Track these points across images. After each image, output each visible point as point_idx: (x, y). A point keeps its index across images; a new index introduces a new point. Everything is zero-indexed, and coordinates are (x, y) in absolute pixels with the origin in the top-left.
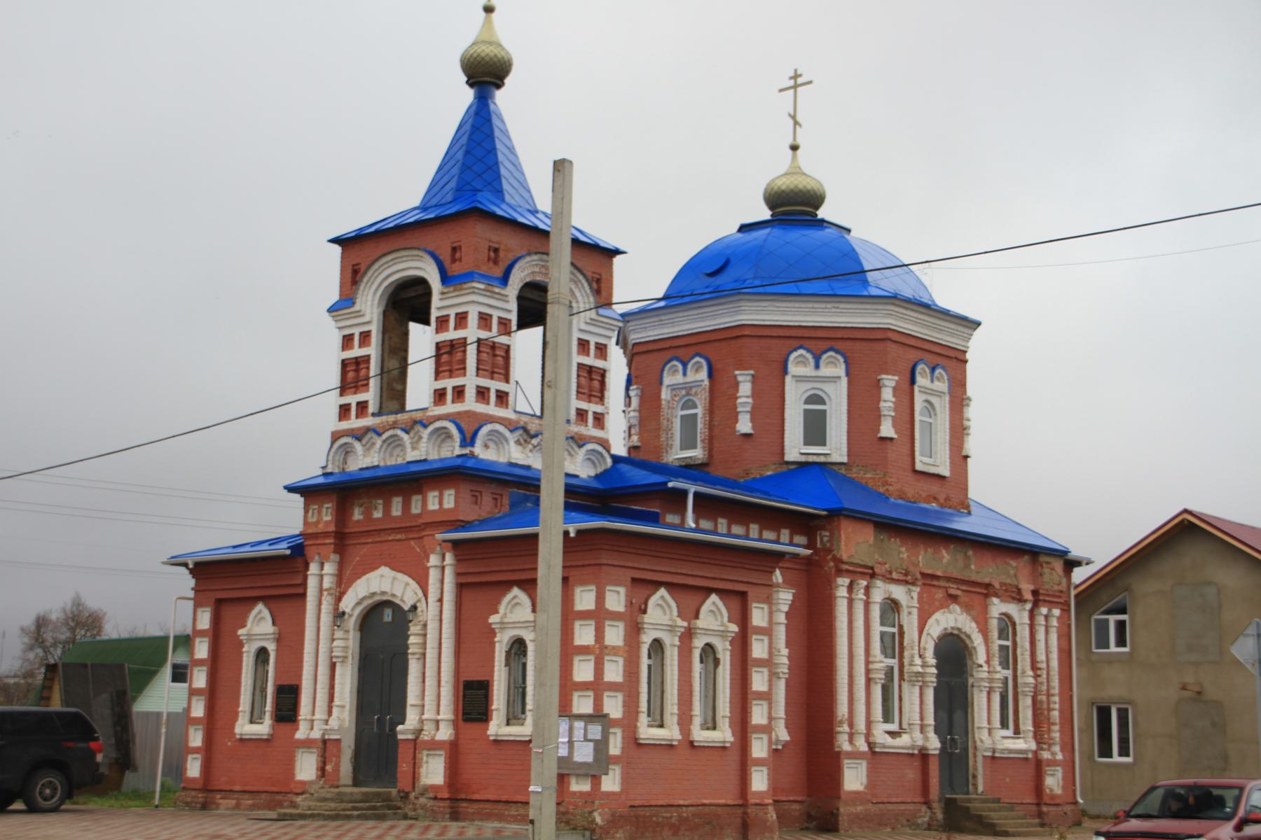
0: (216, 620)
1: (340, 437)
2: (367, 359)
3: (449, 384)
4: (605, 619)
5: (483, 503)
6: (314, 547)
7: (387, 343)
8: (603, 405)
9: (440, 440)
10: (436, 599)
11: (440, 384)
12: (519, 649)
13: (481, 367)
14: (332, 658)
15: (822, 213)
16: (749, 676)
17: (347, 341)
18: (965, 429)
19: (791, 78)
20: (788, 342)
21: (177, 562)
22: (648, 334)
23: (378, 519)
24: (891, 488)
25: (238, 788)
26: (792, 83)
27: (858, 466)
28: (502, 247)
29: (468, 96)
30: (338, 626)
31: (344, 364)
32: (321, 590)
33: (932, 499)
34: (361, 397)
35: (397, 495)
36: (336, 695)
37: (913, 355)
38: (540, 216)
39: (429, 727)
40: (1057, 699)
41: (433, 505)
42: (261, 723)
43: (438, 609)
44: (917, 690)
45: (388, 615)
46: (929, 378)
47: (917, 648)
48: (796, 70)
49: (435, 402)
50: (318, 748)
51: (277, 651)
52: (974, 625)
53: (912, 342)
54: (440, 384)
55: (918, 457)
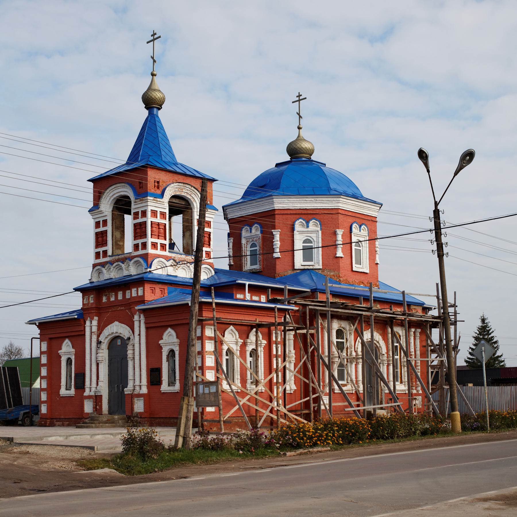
0: (49, 347)
1: (96, 266)
2: (106, 232)
3: (140, 241)
4: (206, 340)
5: (156, 292)
6: (87, 314)
7: (114, 224)
8: (210, 248)
9: (137, 266)
10: (137, 335)
11: (136, 242)
12: (172, 354)
13: (153, 234)
14: (97, 361)
15: (313, 158)
16: (272, 362)
17: (97, 224)
18: (376, 252)
19: (297, 97)
20: (295, 216)
21: (31, 322)
22: (260, 209)
23: (113, 301)
24: (341, 279)
25: (62, 417)
26: (298, 99)
27: (327, 270)
28: (161, 181)
29: (146, 113)
30: (99, 348)
31: (97, 234)
32: (91, 333)
33: (361, 283)
34: (104, 249)
35: (120, 290)
36: (100, 377)
37: (351, 220)
38: (179, 166)
39: (137, 388)
40: (419, 367)
41: (134, 294)
42: (70, 390)
43: (139, 338)
44: (354, 366)
45: (119, 342)
46: (359, 230)
47: (354, 348)
48: (299, 93)
49: (134, 250)
50: (93, 399)
51: (75, 359)
52: (380, 337)
53: (350, 214)
54: (136, 242)
55: (354, 266)
